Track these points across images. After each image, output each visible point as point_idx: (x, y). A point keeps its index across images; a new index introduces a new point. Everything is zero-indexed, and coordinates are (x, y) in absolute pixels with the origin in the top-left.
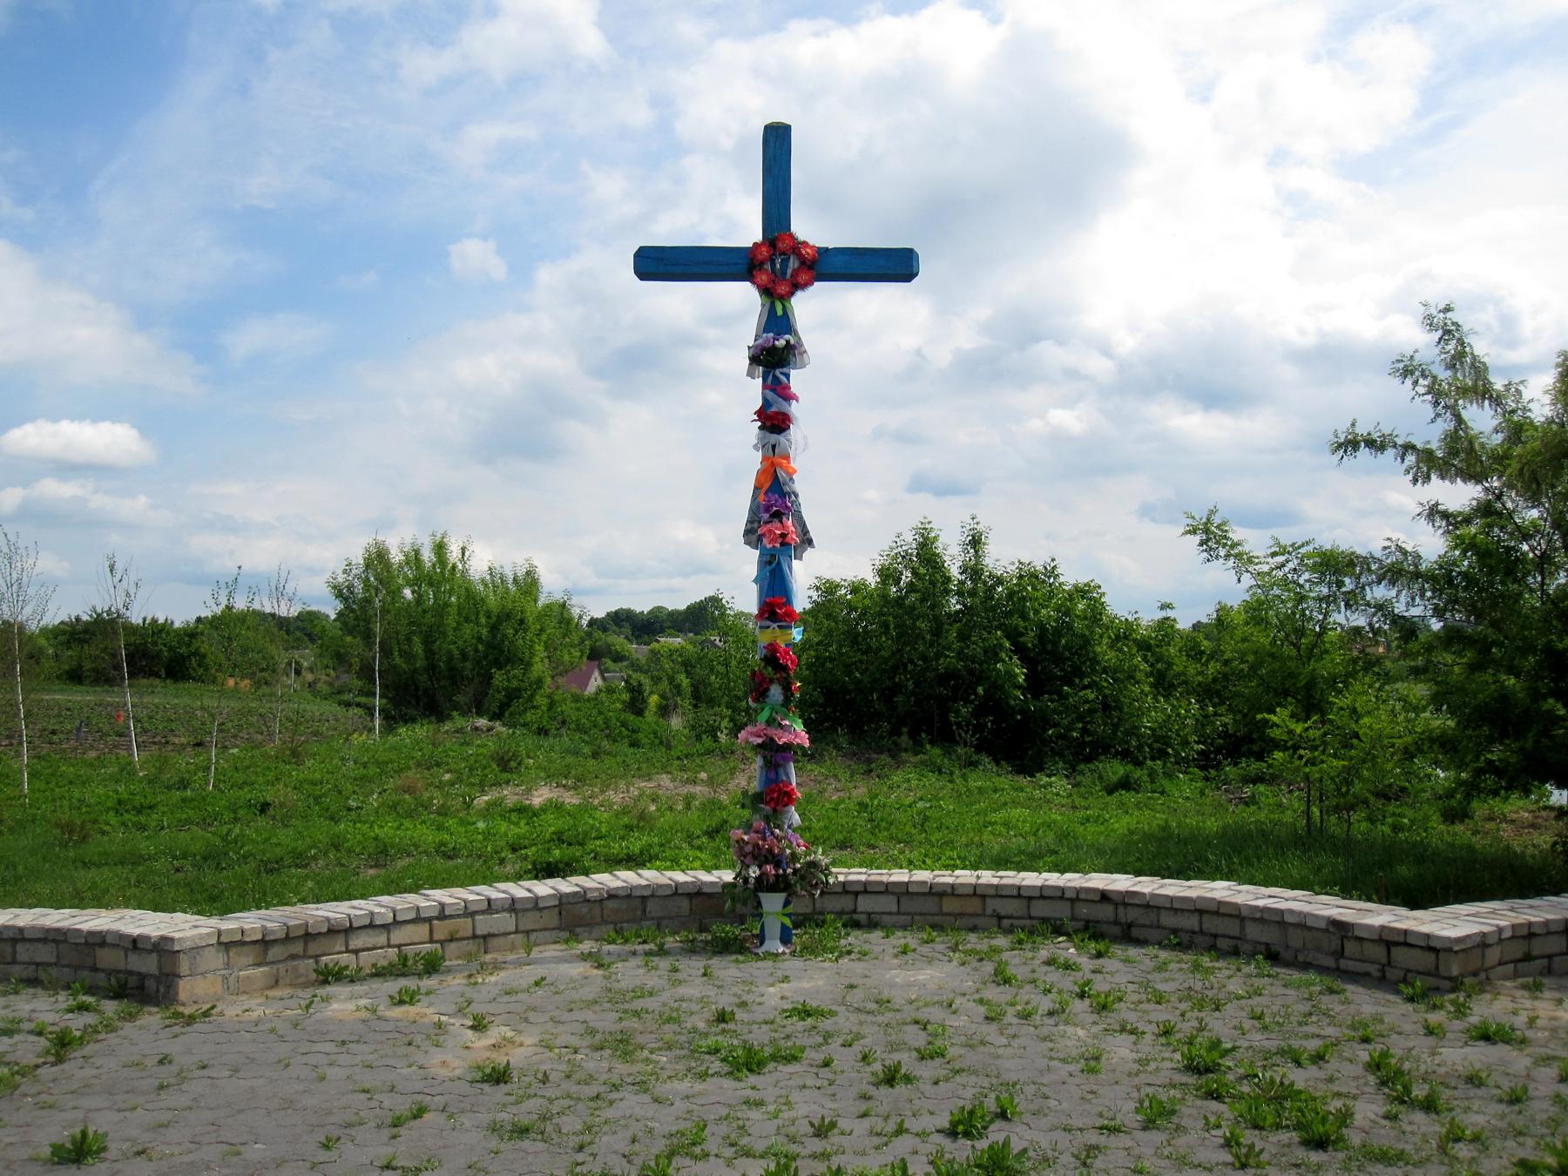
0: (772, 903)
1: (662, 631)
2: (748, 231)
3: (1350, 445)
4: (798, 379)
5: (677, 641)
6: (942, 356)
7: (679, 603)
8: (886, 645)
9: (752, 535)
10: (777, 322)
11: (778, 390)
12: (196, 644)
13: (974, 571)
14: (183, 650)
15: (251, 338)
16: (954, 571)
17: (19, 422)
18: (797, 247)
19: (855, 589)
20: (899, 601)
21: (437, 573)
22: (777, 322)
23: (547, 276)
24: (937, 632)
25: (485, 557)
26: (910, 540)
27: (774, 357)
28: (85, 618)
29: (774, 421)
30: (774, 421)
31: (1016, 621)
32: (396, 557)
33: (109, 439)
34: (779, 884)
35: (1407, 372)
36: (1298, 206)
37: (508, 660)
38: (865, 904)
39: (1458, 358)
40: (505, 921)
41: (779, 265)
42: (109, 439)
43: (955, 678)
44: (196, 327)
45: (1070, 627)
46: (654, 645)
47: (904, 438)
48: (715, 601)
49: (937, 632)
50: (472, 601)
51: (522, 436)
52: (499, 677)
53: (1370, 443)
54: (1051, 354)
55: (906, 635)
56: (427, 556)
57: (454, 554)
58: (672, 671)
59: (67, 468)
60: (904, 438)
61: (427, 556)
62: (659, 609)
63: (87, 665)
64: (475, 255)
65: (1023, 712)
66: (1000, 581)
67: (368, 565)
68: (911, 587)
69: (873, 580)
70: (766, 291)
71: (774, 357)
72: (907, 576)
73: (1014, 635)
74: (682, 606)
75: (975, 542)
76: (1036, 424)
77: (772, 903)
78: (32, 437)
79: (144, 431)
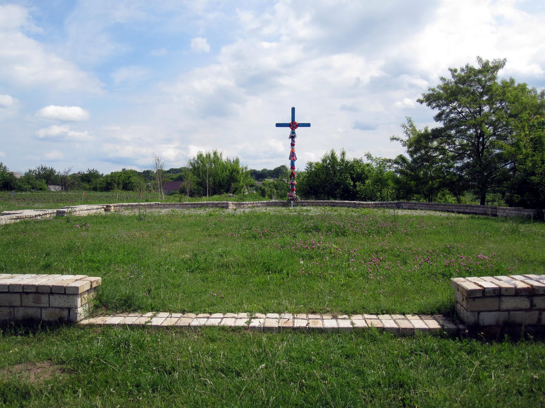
0: (292, 202)
1: (266, 177)
2: (290, 121)
3: (393, 139)
4: (295, 139)
5: (271, 180)
6: (366, 79)
7: (271, 167)
8: (323, 177)
9: (290, 159)
10: (293, 133)
11: (293, 141)
12: (130, 179)
13: (342, 160)
14: (127, 181)
15: (121, 75)
16: (339, 160)
17: (45, 106)
18: (296, 123)
19: (317, 164)
20: (327, 167)
21: (216, 159)
22: (293, 133)
23: (226, 50)
24: (335, 173)
25: (227, 155)
26: (329, 154)
27: (293, 137)
28: (86, 173)
29: (293, 145)
30: (293, 145)
31: (352, 172)
32: (204, 155)
33: (75, 112)
34: (293, 200)
35: (403, 126)
36: (499, 20)
37: (235, 181)
38: (304, 204)
39: (411, 125)
40: (261, 205)
41: (293, 125)
42: (75, 112)
43: (334, 182)
44: (104, 70)
45: (364, 173)
46: (264, 182)
47: (352, 109)
48: (490, 69)
49: (335, 173)
50: (224, 167)
51: (216, 109)
52: (233, 185)
53: (395, 139)
54: (406, 78)
55: (328, 174)
56: (212, 156)
57: (219, 154)
58: (274, 183)
59: (62, 121)
60: (352, 109)
61: (212, 156)
62: (265, 170)
63: (98, 186)
64: (201, 44)
65: (353, 192)
66: (348, 163)
67: (198, 158)
68: (329, 164)
69: (321, 162)
70: (292, 129)
71: (293, 137)
72: (328, 161)
73: (351, 175)
74: (273, 169)
75: (343, 154)
76: (399, 104)
77: (292, 202)
78: (51, 110)
79: (82, 107)
